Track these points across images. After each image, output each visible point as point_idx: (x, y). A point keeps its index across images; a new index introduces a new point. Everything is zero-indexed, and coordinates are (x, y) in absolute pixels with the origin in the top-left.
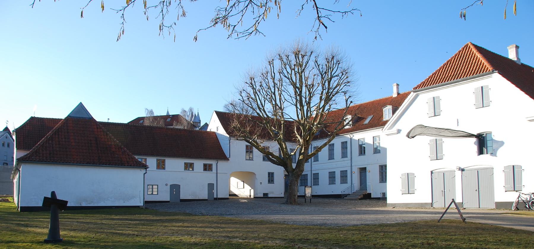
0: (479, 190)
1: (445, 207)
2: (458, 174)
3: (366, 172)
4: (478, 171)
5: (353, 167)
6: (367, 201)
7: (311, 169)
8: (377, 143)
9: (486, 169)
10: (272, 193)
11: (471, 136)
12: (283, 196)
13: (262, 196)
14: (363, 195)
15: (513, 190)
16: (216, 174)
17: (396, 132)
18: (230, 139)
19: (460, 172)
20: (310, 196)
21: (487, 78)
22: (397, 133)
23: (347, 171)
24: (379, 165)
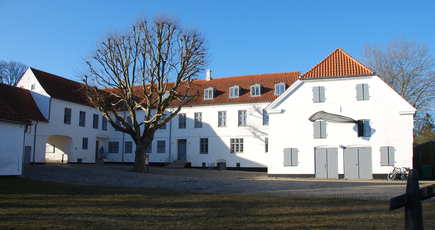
0: (359, 164)
1: (327, 178)
2: (340, 152)
3: (186, 143)
4: (358, 149)
5: (172, 139)
6: (188, 170)
7: (123, 137)
8: (198, 118)
9: (365, 148)
10: (86, 159)
11: (354, 121)
12: (95, 162)
13: (77, 162)
14: (185, 163)
15: (388, 165)
16: (34, 136)
17: (280, 112)
18: (51, 100)
19: (342, 149)
20: (148, 164)
21: (368, 78)
22: (281, 113)
23: (165, 141)
24: (200, 138)
